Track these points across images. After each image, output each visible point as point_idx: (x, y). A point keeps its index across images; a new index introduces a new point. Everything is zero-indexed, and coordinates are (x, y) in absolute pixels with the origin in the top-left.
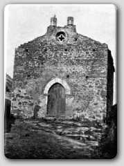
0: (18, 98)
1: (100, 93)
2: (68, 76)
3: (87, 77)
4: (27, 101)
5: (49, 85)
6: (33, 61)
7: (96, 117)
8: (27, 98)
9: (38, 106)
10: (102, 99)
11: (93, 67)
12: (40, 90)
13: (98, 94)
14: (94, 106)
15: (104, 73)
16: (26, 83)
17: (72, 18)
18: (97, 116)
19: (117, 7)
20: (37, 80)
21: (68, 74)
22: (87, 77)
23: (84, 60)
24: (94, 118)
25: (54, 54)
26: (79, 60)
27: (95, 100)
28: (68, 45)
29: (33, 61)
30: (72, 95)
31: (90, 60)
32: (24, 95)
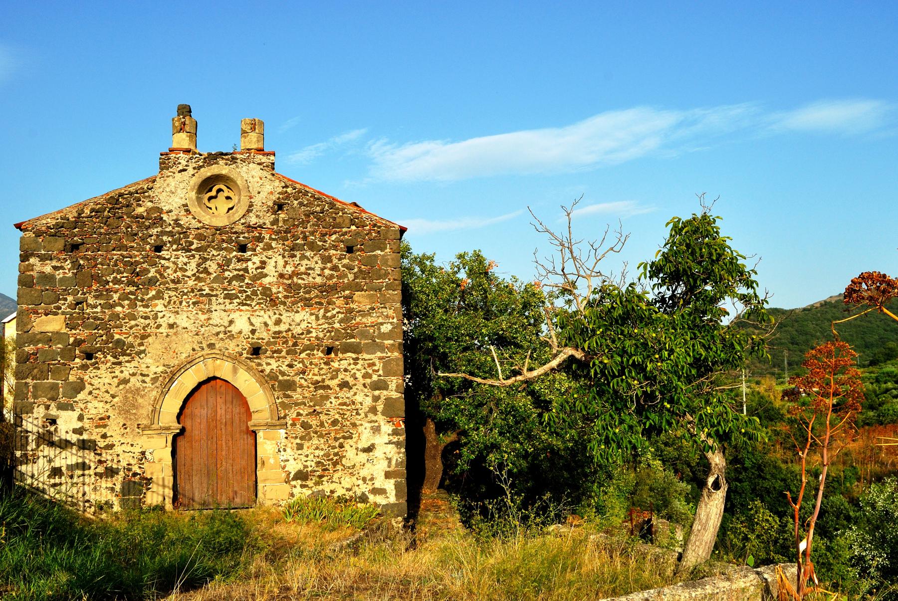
0: (47, 450)
1: (380, 407)
2: (256, 351)
3: (329, 350)
7: (372, 498)
10: (387, 428)
12: (146, 410)
13: (373, 410)
14: (363, 456)
16: (79, 387)
17: (262, 123)
20: (128, 369)
26: (299, 287)
27: (365, 437)
30: (279, 422)
31: (334, 289)
32: (74, 438)
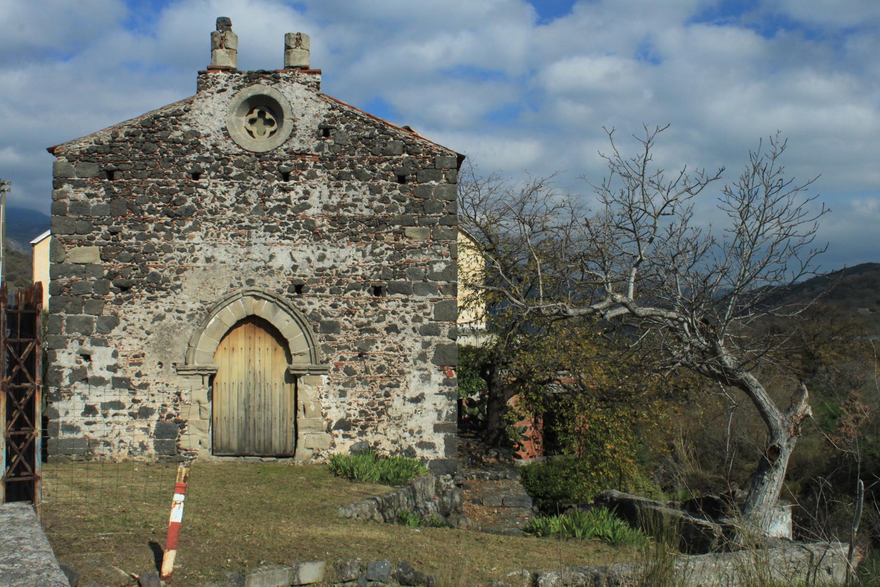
0: (80, 387)
1: (431, 354)
2: (298, 289)
3: (377, 291)
4: (124, 397)
6: (139, 223)
8: (120, 383)
9: (311, 316)
13: (423, 357)
14: (410, 407)
16: (113, 322)
18: (423, 445)
19: (239, 324)
20: (163, 305)
23: (362, 220)
25: (233, 192)
28: (293, 154)
29: (139, 223)
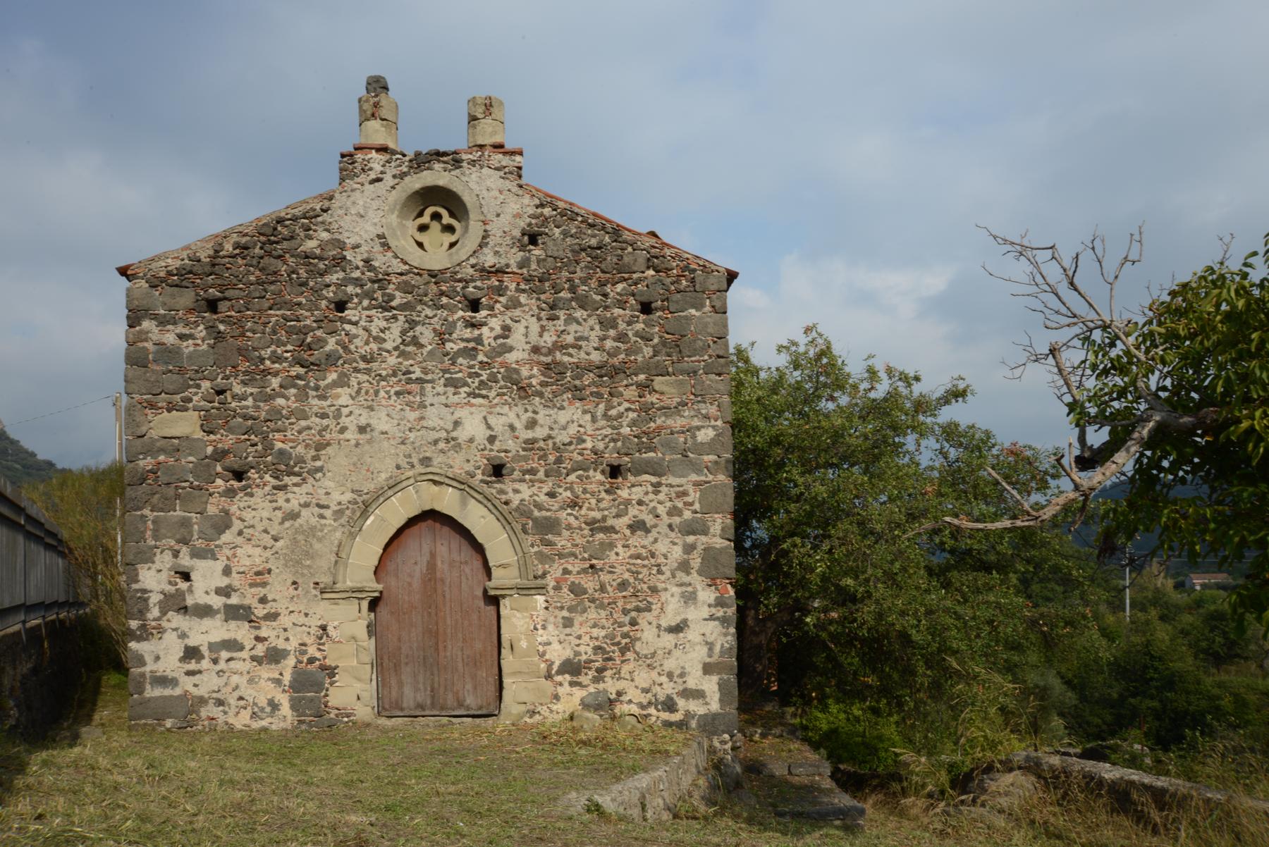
1: (696, 562)
2: (498, 471)
3: (615, 471)
5: (389, 723)
7: (681, 703)
11: (646, 409)
13: (684, 566)
14: (668, 640)
15: (710, 447)
16: (223, 523)
21: (495, 451)
22: (615, 471)
23: (590, 367)
24: (670, 706)
25: (396, 328)
27: (672, 607)
